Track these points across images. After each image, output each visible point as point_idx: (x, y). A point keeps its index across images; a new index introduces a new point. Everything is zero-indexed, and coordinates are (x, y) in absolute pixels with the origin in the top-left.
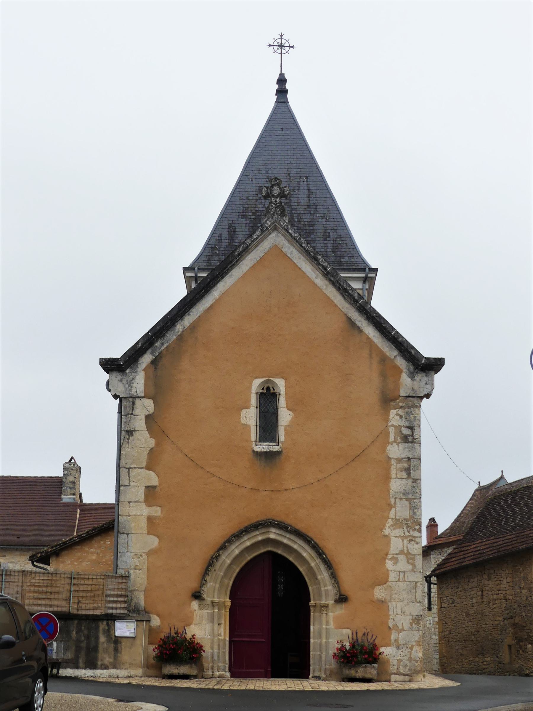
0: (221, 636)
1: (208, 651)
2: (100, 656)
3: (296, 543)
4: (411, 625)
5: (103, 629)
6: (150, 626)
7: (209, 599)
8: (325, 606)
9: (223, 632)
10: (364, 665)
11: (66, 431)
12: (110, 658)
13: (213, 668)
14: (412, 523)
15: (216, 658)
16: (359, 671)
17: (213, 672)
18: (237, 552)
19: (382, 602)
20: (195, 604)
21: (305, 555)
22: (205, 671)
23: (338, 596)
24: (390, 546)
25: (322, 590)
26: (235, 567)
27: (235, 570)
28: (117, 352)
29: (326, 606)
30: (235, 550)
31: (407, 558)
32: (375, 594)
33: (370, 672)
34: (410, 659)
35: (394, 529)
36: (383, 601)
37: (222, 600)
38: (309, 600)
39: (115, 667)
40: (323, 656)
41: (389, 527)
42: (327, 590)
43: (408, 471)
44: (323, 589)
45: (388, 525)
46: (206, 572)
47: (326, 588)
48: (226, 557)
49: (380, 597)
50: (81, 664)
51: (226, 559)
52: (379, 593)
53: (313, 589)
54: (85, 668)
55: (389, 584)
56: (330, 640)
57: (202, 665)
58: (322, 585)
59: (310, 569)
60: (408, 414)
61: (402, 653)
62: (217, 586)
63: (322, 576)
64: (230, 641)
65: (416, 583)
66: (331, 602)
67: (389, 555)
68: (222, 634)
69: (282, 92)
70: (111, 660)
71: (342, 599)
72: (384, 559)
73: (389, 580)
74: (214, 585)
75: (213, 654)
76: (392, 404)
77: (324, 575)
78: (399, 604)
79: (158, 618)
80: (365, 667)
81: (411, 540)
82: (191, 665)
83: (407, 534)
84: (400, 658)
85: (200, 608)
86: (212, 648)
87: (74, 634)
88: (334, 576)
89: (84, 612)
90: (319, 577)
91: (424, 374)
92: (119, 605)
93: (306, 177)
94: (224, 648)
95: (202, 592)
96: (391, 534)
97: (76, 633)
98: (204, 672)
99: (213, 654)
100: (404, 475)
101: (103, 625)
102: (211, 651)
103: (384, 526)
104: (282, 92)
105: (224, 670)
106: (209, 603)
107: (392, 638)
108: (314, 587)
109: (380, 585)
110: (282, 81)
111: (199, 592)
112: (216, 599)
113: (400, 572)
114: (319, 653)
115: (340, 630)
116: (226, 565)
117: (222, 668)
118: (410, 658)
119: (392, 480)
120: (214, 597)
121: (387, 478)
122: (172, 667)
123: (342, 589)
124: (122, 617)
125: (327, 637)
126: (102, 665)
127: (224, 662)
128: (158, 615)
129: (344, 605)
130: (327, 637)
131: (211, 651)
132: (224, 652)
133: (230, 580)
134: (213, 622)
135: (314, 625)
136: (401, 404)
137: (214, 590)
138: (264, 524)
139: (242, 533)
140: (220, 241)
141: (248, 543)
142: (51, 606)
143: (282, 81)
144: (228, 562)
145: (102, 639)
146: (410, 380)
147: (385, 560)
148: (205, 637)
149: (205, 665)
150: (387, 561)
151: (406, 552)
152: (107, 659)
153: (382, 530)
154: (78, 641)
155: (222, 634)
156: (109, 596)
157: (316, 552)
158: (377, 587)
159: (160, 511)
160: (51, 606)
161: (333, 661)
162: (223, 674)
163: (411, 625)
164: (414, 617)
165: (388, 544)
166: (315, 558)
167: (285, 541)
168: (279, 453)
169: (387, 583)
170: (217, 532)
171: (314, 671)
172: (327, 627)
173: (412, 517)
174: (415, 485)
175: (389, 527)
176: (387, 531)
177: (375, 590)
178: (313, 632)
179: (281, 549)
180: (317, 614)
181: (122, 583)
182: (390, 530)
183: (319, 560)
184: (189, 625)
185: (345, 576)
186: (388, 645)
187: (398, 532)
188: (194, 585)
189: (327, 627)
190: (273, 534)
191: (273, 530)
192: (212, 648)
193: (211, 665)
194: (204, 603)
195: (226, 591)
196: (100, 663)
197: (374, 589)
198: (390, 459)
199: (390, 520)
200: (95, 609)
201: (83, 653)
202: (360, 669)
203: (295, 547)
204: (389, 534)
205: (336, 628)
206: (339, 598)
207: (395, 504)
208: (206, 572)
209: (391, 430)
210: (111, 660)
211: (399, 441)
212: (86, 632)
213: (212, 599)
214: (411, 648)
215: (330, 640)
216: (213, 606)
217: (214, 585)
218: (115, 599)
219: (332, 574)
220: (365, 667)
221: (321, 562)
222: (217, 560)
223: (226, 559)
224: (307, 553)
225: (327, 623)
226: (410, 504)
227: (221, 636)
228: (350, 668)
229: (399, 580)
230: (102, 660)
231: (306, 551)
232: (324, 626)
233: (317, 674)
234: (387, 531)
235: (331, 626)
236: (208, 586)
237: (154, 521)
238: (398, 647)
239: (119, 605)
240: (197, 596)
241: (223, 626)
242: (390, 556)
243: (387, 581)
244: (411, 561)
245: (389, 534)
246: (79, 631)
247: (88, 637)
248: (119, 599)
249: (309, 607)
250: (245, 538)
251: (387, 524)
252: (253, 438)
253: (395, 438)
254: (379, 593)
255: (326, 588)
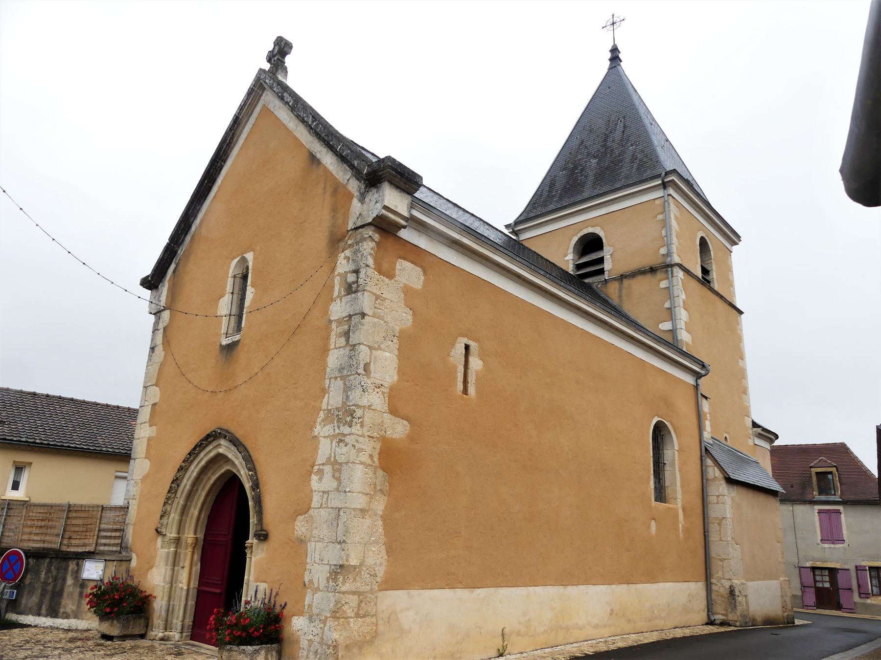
1: (159, 605)
2: (63, 602)
4: (328, 582)
5: (73, 570)
9: (186, 578)
10: (228, 647)
11: (105, 353)
12: (73, 605)
14: (343, 414)
24: (317, 453)
28: (147, 270)
31: (333, 469)
34: (322, 642)
35: (324, 425)
39: (76, 617)
43: (347, 334)
45: (319, 420)
50: (43, 611)
54: (46, 616)
55: (311, 511)
60: (355, 253)
61: (314, 629)
65: (340, 509)
69: (615, 57)
70: (74, 608)
72: (310, 473)
76: (342, 244)
78: (319, 545)
81: (341, 441)
82: (113, 621)
83: (337, 431)
84: (311, 637)
87: (43, 575)
89: (72, 549)
91: (374, 190)
92: (113, 541)
93: (624, 117)
96: (322, 434)
97: (46, 574)
100: (343, 341)
101: (72, 565)
103: (315, 422)
104: (615, 57)
107: (306, 603)
110: (615, 51)
113: (324, 492)
118: (322, 639)
119: (331, 352)
121: (325, 350)
124: (90, 555)
126: (64, 613)
136: (350, 242)
140: (541, 196)
142: (44, 542)
143: (615, 51)
145: (70, 581)
146: (360, 204)
151: (332, 459)
152: (70, 606)
154: (45, 583)
156: (104, 530)
160: (44, 542)
163: (328, 582)
164: (333, 567)
165: (315, 450)
168: (238, 342)
173: (344, 403)
174: (352, 353)
176: (317, 430)
181: (7, 515)
186: (300, 613)
187: (328, 430)
191: (223, 442)
196: (62, 610)
198: (330, 321)
200: (85, 545)
201: (48, 597)
207: (329, 387)
209: (337, 280)
210: (74, 608)
211: (343, 293)
212: (54, 572)
214: (324, 622)
218: (109, 534)
226: (345, 384)
229: (321, 507)
230: (65, 607)
238: (311, 619)
239: (113, 541)
243: (309, 508)
244: (337, 475)
246: (49, 571)
247: (55, 579)
248: (114, 534)
252: (224, 330)
253: (339, 292)
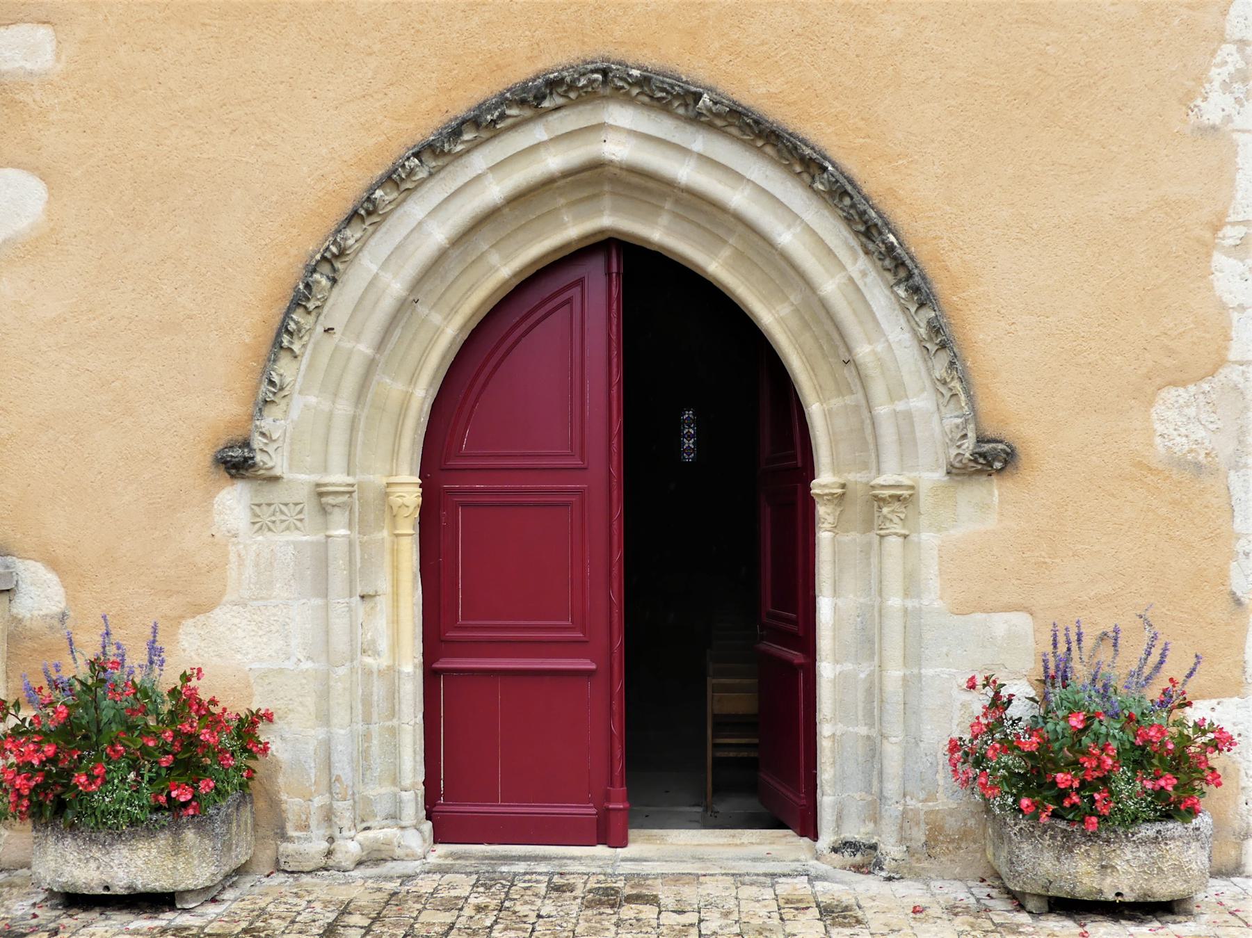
0: (377, 653)
3: (740, 177)
6: (17, 620)
7: (303, 477)
8: (898, 498)
9: (392, 631)
10: (1147, 831)
13: (329, 816)
15: (342, 767)
16: (1121, 865)
17: (331, 839)
18: (439, 235)
19: (1197, 469)
20: (233, 500)
21: (786, 237)
22: (291, 832)
23: (969, 445)
25: (870, 415)
26: (436, 318)
27: (438, 331)
29: (904, 499)
30: (428, 220)
32: (1160, 428)
33: (1178, 868)
36: (1198, 467)
37: (379, 479)
38: (807, 470)
40: (892, 751)
41: (1226, 86)
42: (908, 415)
44: (883, 410)
45: (1217, 75)
46: (281, 340)
47: (900, 406)
48: (384, 265)
49: (1181, 444)
51: (386, 277)
52: (1177, 422)
53: (828, 415)
55: (1231, 374)
56: (928, 672)
57: (274, 804)
58: (878, 389)
59: (819, 315)
62: (344, 408)
63: (880, 347)
64: (431, 676)
66: (929, 477)
67: (1228, 231)
68: (383, 645)
71: (991, 459)
72: (1207, 249)
73: (1232, 356)
74: (326, 406)
75: (327, 747)
77: (885, 334)
79: (51, 577)
80: (1155, 841)
85: (258, 525)
86: (325, 718)
88: (940, 338)
90: (863, 351)
94: (393, 712)
95: (258, 442)
98: (284, 837)
99: (327, 747)
102: (321, 733)
103: (1201, 79)
105: (394, 817)
106: (302, 494)
108: (836, 403)
109: (1184, 384)
111: (246, 444)
112: (337, 478)
114: (863, 730)
115: (979, 616)
116: (387, 304)
117: (383, 808)
120: (325, 469)
122: (72, 856)
123: (983, 405)
125: (913, 656)
127: (395, 780)
128: (53, 564)
129: (993, 491)
130: (913, 656)
131: (321, 733)
132: (394, 732)
133: (413, 379)
134: (323, 590)
135: (836, 592)
137: (329, 429)
138: (572, 86)
139: (455, 133)
141: (495, 191)
144: (396, 286)
147: (1209, 255)
148: (289, 665)
149: (292, 804)
150: (1218, 259)
153: (1187, 100)
155: (383, 645)
157: (848, 220)
158: (1170, 394)
159: (49, 48)
161: (943, 777)
162: (388, 843)
166: (843, 255)
167: (685, 173)
169: (1223, 371)
170: (340, 143)
171: (839, 818)
172: (910, 604)
175: (1226, 86)
176: (1214, 107)
177: (1158, 409)
178: (836, 628)
179: (664, 219)
180: (852, 538)
182: (1229, 99)
183: (863, 262)
184: (201, 607)
185: (988, 335)
188: (216, 410)
189: (910, 604)
190: (624, 135)
191: (621, 115)
192: (325, 718)
193: (318, 801)
194: (276, 494)
195: (398, 435)
197: (1151, 403)
199: (1231, 48)
202: (1128, 852)
203: (737, 199)
204: (1228, 119)
205: (962, 610)
206: (978, 455)
208: (281, 340)
213: (316, 478)
215: (928, 672)
216: (324, 511)
217: (326, 406)
219: (935, 329)
220: (1155, 841)
221: (873, 275)
222: (334, 281)
223: (386, 277)
224: (798, 223)
225: (911, 585)
227: (377, 653)
228: (1067, 845)
231: (794, 217)
232: (895, 602)
233: (857, 832)
234: (1214, 107)
235: (933, 598)
236: (295, 414)
237: (21, 96)
240: (236, 463)
241: (383, 603)
242: (1231, 234)
243: (1222, 362)
245: (1228, 119)
249: (809, 504)
250: (480, 161)
251: (1214, 71)
254: (1177, 422)
255: (900, 406)
